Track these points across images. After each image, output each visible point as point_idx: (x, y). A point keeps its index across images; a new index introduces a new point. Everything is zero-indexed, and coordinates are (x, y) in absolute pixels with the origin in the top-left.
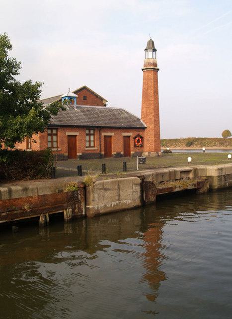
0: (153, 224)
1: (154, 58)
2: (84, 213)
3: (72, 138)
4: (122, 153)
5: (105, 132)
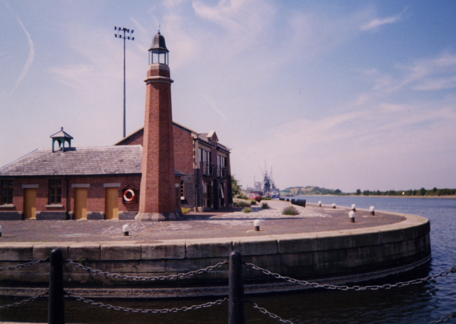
5: (76, 183)
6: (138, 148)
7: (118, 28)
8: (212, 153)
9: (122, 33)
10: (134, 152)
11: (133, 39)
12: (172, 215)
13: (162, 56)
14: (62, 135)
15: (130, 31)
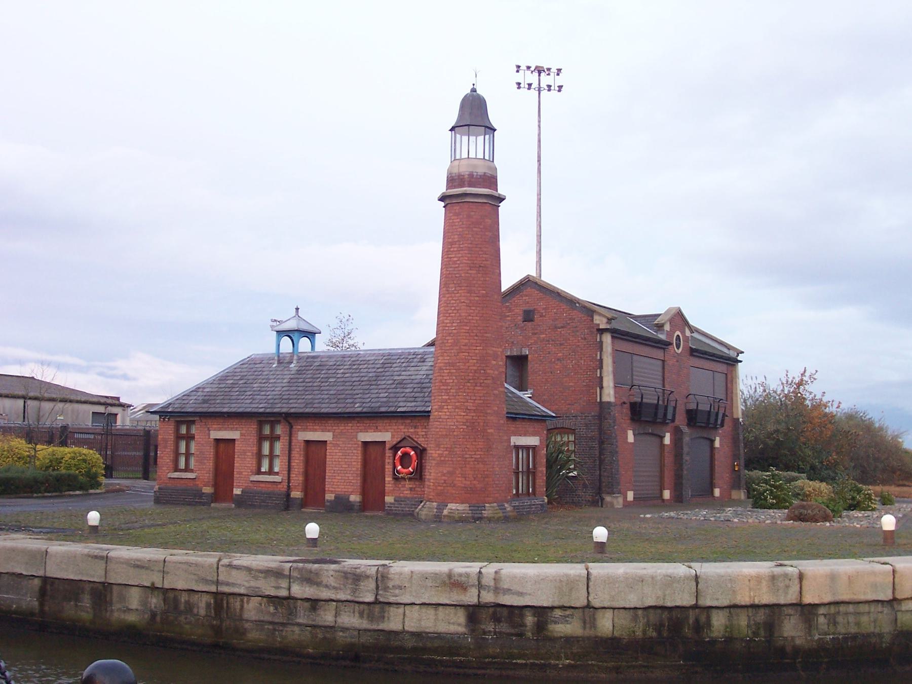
4: (355, 498)
7: (523, 67)
9: (533, 78)
11: (560, 87)
14: (291, 325)
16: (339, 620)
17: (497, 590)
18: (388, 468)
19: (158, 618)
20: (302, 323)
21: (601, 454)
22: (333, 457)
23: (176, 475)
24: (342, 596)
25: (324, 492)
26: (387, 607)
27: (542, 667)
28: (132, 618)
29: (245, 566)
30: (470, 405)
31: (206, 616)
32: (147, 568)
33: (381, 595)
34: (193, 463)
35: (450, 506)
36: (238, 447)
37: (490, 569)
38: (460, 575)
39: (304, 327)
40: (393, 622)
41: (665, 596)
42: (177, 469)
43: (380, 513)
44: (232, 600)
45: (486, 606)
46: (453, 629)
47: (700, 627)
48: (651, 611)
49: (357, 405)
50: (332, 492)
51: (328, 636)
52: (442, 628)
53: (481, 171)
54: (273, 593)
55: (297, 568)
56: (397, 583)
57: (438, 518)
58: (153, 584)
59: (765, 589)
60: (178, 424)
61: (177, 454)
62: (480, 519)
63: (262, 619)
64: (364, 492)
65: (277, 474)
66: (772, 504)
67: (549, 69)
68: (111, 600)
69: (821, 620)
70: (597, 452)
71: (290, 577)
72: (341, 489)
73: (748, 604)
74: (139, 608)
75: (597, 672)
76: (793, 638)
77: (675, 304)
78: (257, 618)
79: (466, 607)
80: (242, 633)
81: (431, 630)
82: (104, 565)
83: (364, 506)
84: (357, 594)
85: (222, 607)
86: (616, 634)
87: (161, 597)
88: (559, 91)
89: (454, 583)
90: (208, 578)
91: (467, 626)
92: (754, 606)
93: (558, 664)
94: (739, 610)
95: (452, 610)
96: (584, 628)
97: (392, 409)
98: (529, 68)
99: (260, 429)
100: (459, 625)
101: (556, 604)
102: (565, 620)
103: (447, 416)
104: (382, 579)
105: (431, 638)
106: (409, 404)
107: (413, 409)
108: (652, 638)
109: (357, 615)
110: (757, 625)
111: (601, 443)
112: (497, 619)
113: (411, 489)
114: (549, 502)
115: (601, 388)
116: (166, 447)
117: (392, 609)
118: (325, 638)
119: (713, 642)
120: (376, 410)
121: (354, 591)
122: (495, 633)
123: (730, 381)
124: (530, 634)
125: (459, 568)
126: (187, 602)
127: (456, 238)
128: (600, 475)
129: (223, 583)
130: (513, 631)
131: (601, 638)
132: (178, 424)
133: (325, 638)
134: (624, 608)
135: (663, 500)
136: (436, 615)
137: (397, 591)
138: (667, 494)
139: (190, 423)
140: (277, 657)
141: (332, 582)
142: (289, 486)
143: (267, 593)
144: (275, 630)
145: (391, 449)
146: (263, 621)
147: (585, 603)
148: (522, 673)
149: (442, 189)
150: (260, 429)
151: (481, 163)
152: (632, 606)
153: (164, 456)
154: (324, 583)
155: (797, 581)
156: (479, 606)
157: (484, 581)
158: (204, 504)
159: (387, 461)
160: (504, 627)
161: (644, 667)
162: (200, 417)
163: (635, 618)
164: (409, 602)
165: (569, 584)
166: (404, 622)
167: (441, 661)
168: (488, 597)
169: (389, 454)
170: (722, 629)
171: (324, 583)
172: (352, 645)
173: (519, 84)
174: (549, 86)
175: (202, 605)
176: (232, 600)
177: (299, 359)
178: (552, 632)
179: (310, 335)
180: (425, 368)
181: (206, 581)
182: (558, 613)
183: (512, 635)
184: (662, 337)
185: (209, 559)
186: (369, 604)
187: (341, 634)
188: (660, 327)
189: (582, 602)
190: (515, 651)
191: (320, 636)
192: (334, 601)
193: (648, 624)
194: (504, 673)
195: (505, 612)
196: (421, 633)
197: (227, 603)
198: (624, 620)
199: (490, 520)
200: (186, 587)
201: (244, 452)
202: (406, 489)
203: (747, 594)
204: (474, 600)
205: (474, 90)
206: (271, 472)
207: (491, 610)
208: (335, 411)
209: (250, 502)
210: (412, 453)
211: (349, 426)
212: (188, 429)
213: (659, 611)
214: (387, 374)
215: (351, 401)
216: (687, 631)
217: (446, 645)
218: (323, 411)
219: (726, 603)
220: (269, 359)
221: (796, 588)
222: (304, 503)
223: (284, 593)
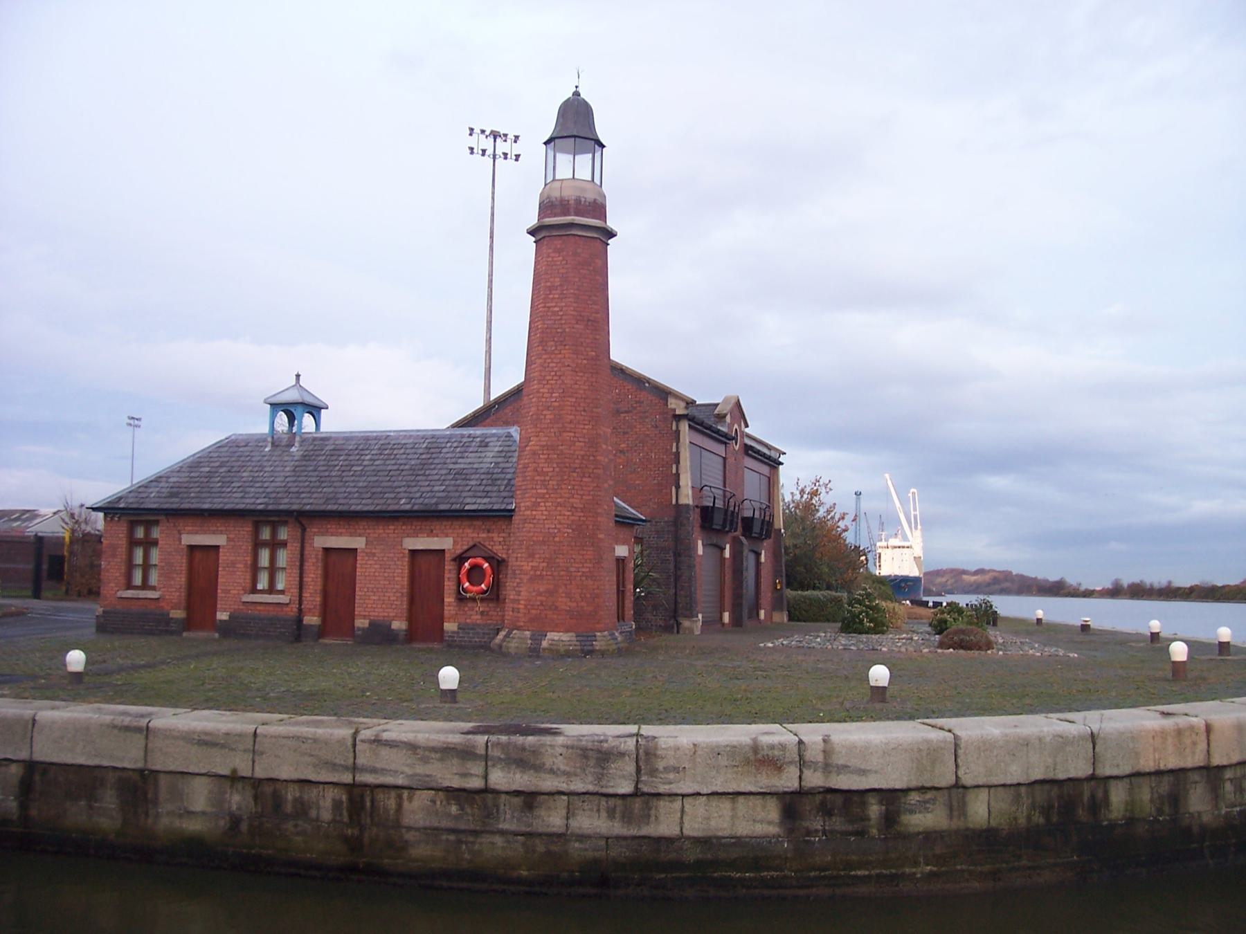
0: (894, 542)
1: (597, 181)
2: (674, 502)
3: (201, 558)
4: (399, 625)
5: (325, 533)
6: (509, 436)
8: (730, 461)
9: (488, 144)
10: (495, 447)
11: (517, 157)
12: (268, 789)
13: (584, 160)
14: (293, 396)
15: (511, 136)
16: (574, 823)
17: (827, 767)
18: (449, 586)
19: (244, 827)
20: (305, 394)
21: (677, 568)
22: (366, 570)
23: (129, 593)
24: (578, 786)
25: (352, 618)
26: (654, 802)
27: (893, 877)
28: (194, 826)
29: (409, 738)
30: (576, 501)
31: (334, 821)
32: (223, 746)
33: (645, 783)
34: (154, 578)
35: (550, 635)
36: (223, 557)
37: (812, 733)
38: (772, 747)
39: (309, 400)
40: (665, 824)
41: (1055, 764)
42: (129, 586)
43: (436, 646)
44: (380, 796)
45: (811, 792)
46: (760, 829)
47: (1098, 805)
48: (1037, 787)
49: (403, 501)
50: (364, 617)
51: (553, 848)
52: (744, 829)
53: (590, 196)
54: (456, 783)
55: (498, 744)
56: (672, 762)
57: (535, 652)
58: (234, 771)
59: (1170, 749)
60: (132, 525)
61: (130, 566)
62: (591, 652)
63: (436, 824)
64: (411, 618)
65: (282, 592)
66: (869, 628)
67: (505, 135)
68: (157, 798)
69: (1228, 787)
70: (672, 566)
71: (486, 758)
72: (379, 613)
73: (1153, 770)
74: (209, 809)
75: (967, 881)
76: (1199, 813)
77: (733, 393)
78: (427, 824)
79: (780, 795)
80: (401, 847)
81: (726, 833)
82: (143, 742)
83: (411, 636)
84: (604, 783)
85: (363, 807)
86: (993, 823)
87: (249, 793)
88: (517, 160)
89: (761, 759)
90: (337, 761)
91: (782, 823)
92: (1159, 773)
93: (915, 874)
94: (1140, 780)
95: (758, 801)
96: (951, 817)
97: (457, 507)
98: (483, 132)
99: (256, 532)
100: (770, 823)
101: (914, 784)
102: (923, 806)
103: (541, 516)
104: (646, 757)
105: (724, 845)
106: (479, 501)
107: (489, 507)
108: (1038, 825)
109: (603, 814)
110: (1161, 797)
111: (677, 555)
112: (827, 812)
113: (482, 613)
114: (638, 628)
115: (678, 487)
116: (114, 556)
117: (662, 803)
118: (549, 853)
119: (1113, 825)
120: (433, 508)
121: (599, 778)
122: (824, 832)
123: (772, 483)
124: (874, 831)
125: (774, 735)
126: (299, 802)
127: (557, 281)
128: (676, 594)
129: (364, 770)
130: (850, 828)
131: (974, 831)
132: (132, 525)
133: (549, 853)
134: (1004, 785)
135: (723, 624)
136: (733, 809)
137: (671, 776)
138: (726, 617)
139: (149, 525)
140: (464, 885)
141: (561, 764)
142: (300, 610)
143: (446, 784)
144: (459, 842)
145: (454, 560)
146: (436, 829)
147: (951, 780)
148: (863, 890)
149: (533, 221)
150: (256, 532)
151: (590, 186)
152: (1015, 782)
153: (111, 569)
154: (547, 766)
155: (1203, 737)
156: (801, 793)
157: (809, 755)
158: (172, 633)
159: (447, 576)
160: (838, 823)
161: (1029, 868)
162: (167, 515)
163: (1017, 799)
164: (690, 791)
165: (930, 753)
166: (682, 823)
167: (741, 880)
168: (814, 779)
169: (449, 567)
170: (1122, 807)
171: (547, 766)
172: (596, 861)
173: (472, 149)
174: (505, 155)
175: (325, 806)
176: (380, 796)
177: (303, 441)
178: (917, 825)
179: (315, 410)
180: (491, 454)
181: (334, 767)
182: (914, 797)
183: (851, 834)
184: (724, 429)
185: (334, 730)
186: (623, 796)
187: (577, 845)
188: (721, 417)
189: (947, 779)
190: (854, 858)
191: (541, 848)
192: (563, 793)
193: (1033, 807)
194: (838, 891)
195: (839, 800)
196: (710, 838)
197: (372, 801)
198: (1003, 803)
199: (603, 653)
200: (296, 775)
201: (233, 564)
202: (475, 614)
203: (1151, 756)
204: (793, 785)
205: (577, 94)
206: (271, 589)
207: (818, 798)
208: (371, 508)
209: (246, 630)
210: (486, 565)
211: (389, 531)
212: (147, 532)
213: (1047, 787)
214: (436, 461)
215: (392, 495)
216: (1082, 814)
217: (751, 855)
218: (353, 508)
219: (1127, 770)
220: (258, 441)
221: (1202, 746)
222: (322, 632)
223: (476, 783)
